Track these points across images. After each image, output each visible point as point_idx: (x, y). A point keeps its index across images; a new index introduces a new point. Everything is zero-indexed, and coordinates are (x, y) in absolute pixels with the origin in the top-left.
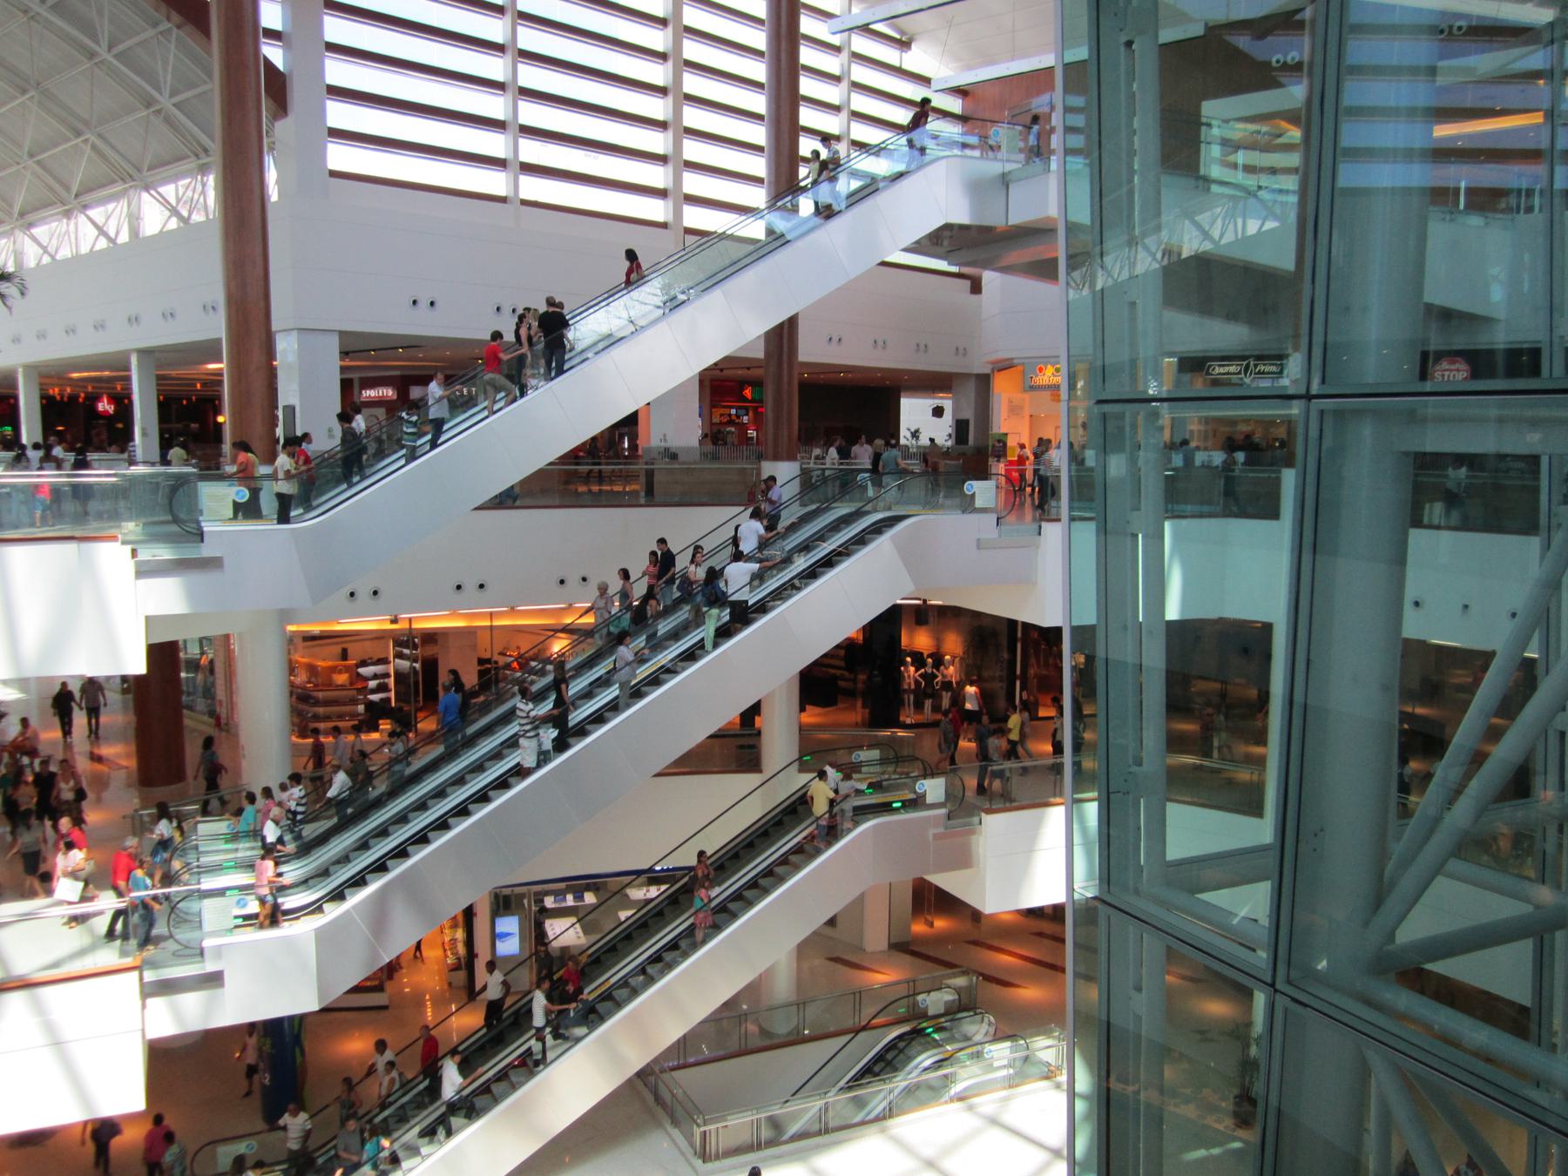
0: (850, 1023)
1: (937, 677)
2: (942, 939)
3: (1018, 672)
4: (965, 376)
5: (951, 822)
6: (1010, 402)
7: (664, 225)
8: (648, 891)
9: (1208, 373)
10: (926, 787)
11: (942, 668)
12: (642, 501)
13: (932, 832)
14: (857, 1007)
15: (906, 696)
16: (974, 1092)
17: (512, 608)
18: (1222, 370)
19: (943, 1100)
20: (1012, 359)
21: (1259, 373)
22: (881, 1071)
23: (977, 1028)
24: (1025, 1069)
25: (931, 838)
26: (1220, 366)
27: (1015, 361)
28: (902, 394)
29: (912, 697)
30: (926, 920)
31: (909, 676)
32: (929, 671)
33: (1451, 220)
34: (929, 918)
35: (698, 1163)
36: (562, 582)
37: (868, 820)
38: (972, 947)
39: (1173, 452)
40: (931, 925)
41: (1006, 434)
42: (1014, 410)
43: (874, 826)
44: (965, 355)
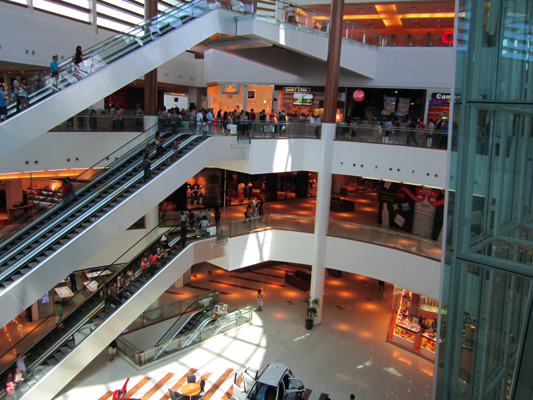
0: (177, 312)
1: (198, 192)
2: (200, 281)
3: (225, 190)
4: (193, 88)
5: (218, 241)
6: (214, 97)
7: (89, 23)
8: (93, 274)
9: (284, 91)
10: (210, 230)
11: (200, 189)
12: (88, 129)
13: (212, 246)
14: (180, 305)
15: (188, 199)
16: (227, 329)
17: (46, 170)
18: (289, 90)
19: (216, 333)
20: (217, 82)
21: (301, 92)
22: (192, 328)
23: (221, 309)
24: (241, 321)
25: (212, 247)
26: (288, 89)
27: (218, 83)
28: (164, 93)
29: (190, 200)
30: (194, 275)
31: (189, 192)
32: (196, 190)
33: (363, 47)
34: (195, 274)
35: (138, 367)
36: (68, 160)
37: (192, 242)
38: (211, 282)
39: (104, 111)
40: (196, 277)
41: (213, 109)
42: (215, 100)
43: (194, 245)
44: (193, 80)
